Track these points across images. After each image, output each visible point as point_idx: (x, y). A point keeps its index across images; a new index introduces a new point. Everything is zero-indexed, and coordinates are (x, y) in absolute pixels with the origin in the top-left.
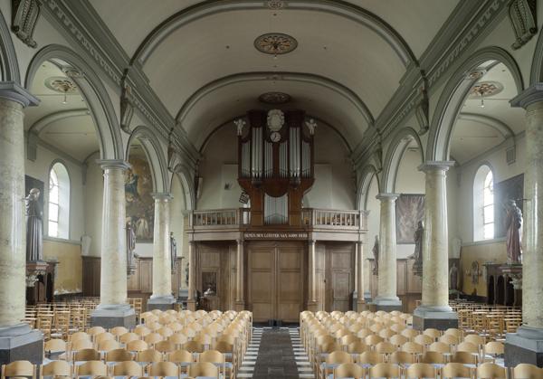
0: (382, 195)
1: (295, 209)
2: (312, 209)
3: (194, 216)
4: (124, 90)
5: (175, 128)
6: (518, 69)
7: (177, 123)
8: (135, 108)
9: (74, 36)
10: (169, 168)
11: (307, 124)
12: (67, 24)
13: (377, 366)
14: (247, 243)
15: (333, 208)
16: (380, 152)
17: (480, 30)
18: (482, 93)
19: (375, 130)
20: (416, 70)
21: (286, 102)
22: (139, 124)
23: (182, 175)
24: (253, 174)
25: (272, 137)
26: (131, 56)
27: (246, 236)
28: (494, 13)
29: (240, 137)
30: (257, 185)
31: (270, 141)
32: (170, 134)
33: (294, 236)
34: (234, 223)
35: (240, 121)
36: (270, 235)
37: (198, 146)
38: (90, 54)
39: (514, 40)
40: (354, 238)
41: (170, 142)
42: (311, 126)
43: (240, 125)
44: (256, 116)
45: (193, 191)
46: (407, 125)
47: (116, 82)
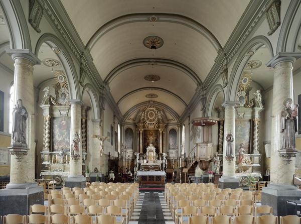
5: (84, 52)
17: (253, 28)
18: (252, 67)
20: (222, 53)
28: (260, 18)
32: (81, 57)
38: (68, 45)
39: (268, 30)
41: (81, 64)
46: (218, 83)
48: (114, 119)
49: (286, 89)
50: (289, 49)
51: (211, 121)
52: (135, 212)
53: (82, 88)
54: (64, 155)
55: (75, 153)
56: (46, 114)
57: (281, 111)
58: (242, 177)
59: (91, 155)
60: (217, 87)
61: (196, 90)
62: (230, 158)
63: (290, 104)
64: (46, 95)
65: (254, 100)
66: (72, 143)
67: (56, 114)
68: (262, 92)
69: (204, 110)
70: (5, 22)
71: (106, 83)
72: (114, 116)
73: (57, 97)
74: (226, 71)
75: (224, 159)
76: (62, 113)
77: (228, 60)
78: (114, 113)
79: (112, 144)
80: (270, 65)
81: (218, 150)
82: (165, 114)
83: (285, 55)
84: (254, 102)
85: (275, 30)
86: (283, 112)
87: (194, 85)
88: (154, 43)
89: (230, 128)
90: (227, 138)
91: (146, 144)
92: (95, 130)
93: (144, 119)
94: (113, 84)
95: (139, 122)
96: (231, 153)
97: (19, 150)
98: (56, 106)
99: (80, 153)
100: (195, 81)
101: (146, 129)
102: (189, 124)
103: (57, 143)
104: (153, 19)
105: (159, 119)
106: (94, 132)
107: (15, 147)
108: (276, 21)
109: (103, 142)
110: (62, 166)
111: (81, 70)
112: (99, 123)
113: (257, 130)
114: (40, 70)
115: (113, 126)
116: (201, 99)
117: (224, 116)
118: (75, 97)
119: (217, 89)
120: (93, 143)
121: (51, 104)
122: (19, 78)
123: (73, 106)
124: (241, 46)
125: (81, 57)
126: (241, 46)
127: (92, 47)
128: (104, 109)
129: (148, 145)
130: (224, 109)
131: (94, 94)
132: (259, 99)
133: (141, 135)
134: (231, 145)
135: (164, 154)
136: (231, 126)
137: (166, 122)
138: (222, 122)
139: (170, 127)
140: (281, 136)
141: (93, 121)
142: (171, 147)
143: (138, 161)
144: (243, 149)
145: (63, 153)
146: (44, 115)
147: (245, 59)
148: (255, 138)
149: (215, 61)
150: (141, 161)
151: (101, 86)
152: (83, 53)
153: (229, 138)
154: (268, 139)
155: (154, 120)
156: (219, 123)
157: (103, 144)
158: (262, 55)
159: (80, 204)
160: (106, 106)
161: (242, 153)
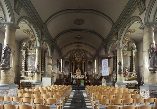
4: (42, 31)
6: (141, 20)
8: (22, 6)
9: (31, 15)
12: (27, 10)
13: (24, 98)
18: (130, 32)
22: (45, 39)
26: (44, 22)
32: (42, 28)
39: (139, 13)
41: (42, 31)
48: (59, 56)
49: (150, 39)
50: (151, 20)
51: (110, 57)
52: (69, 99)
53: (42, 42)
54: (32, 72)
55: (38, 71)
56: (24, 54)
57: (148, 49)
58: (127, 83)
59: (46, 73)
60: (113, 41)
61: (101, 43)
62: (120, 73)
63: (153, 45)
64: (24, 45)
65: (132, 47)
66: (36, 66)
67: (29, 54)
68: (135, 44)
69: (106, 51)
70: (2, 11)
71: (55, 40)
72: (59, 55)
73: (30, 46)
74: (117, 33)
75: (117, 74)
76: (32, 53)
77: (118, 28)
78: (59, 54)
79: (58, 68)
80: (141, 28)
81: (114, 70)
82: (85, 54)
83: (149, 23)
84: (132, 48)
85: (143, 12)
86: (149, 49)
87: (100, 41)
88: (79, 21)
89: (120, 59)
90: (119, 64)
91: (76, 68)
92: (48, 61)
93: (75, 57)
94: (58, 41)
95: (72, 58)
96: (121, 70)
97: (5, 68)
98: (29, 50)
99: (40, 71)
100: (101, 39)
101: (76, 61)
102: (98, 59)
103: (29, 67)
104: (79, 12)
105: (82, 57)
106: (48, 62)
107: (3, 66)
108: (143, 8)
109: (53, 66)
110: (31, 78)
111: (42, 34)
112: (51, 58)
113: (134, 63)
114: (19, 33)
115: (58, 59)
116: (105, 47)
117: (117, 55)
118: (38, 45)
119: (112, 42)
120: (48, 67)
121: (27, 50)
122: (7, 35)
123: (37, 49)
124: (124, 21)
125: (42, 28)
126: (124, 21)
127: (48, 24)
128: (54, 52)
129: (77, 69)
130: (116, 51)
131: (49, 45)
132: (135, 46)
133: (73, 64)
134: (121, 67)
135: (85, 73)
136: (120, 58)
137: (86, 58)
138: (115, 57)
139: (88, 61)
140: (149, 61)
141: (48, 57)
142: (89, 69)
143: (71, 76)
144: (127, 70)
145: (32, 72)
146: (23, 54)
147: (127, 27)
148: (133, 63)
149: (111, 29)
150: (73, 76)
151: (52, 41)
152: (43, 26)
153: (120, 64)
154: (141, 65)
155: (80, 57)
156: (114, 58)
157: (53, 67)
158: (135, 26)
159: (41, 98)
160: (55, 51)
161: (127, 71)
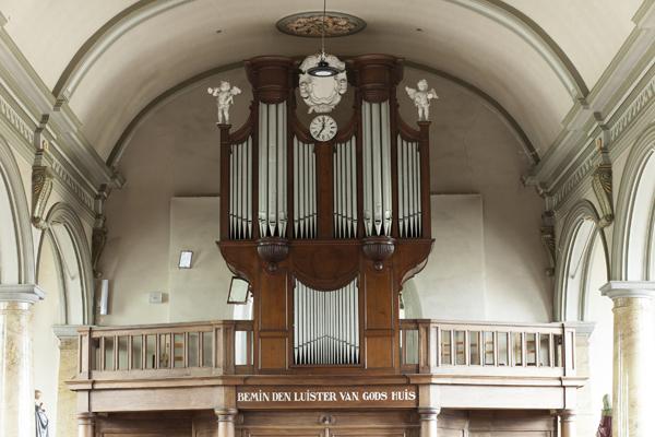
0: (615, 285)
1: (379, 322)
2: (428, 322)
3: (95, 343)
5: (54, 115)
7: (58, 105)
10: (35, 220)
11: (410, 91)
14: (244, 415)
15: (488, 318)
16: (605, 173)
19: (589, 113)
21: (351, 32)
23: (61, 232)
24: (263, 227)
25: (315, 127)
27: (244, 397)
29: (224, 128)
30: (273, 259)
31: (308, 138)
32: (38, 130)
33: (377, 396)
34: (206, 363)
35: (225, 86)
36: (311, 396)
37: (104, 152)
40: (550, 400)
41: (39, 152)
42: (421, 97)
43: (226, 97)
44: (271, 73)
45: (89, 275)
47: (27, 141)
